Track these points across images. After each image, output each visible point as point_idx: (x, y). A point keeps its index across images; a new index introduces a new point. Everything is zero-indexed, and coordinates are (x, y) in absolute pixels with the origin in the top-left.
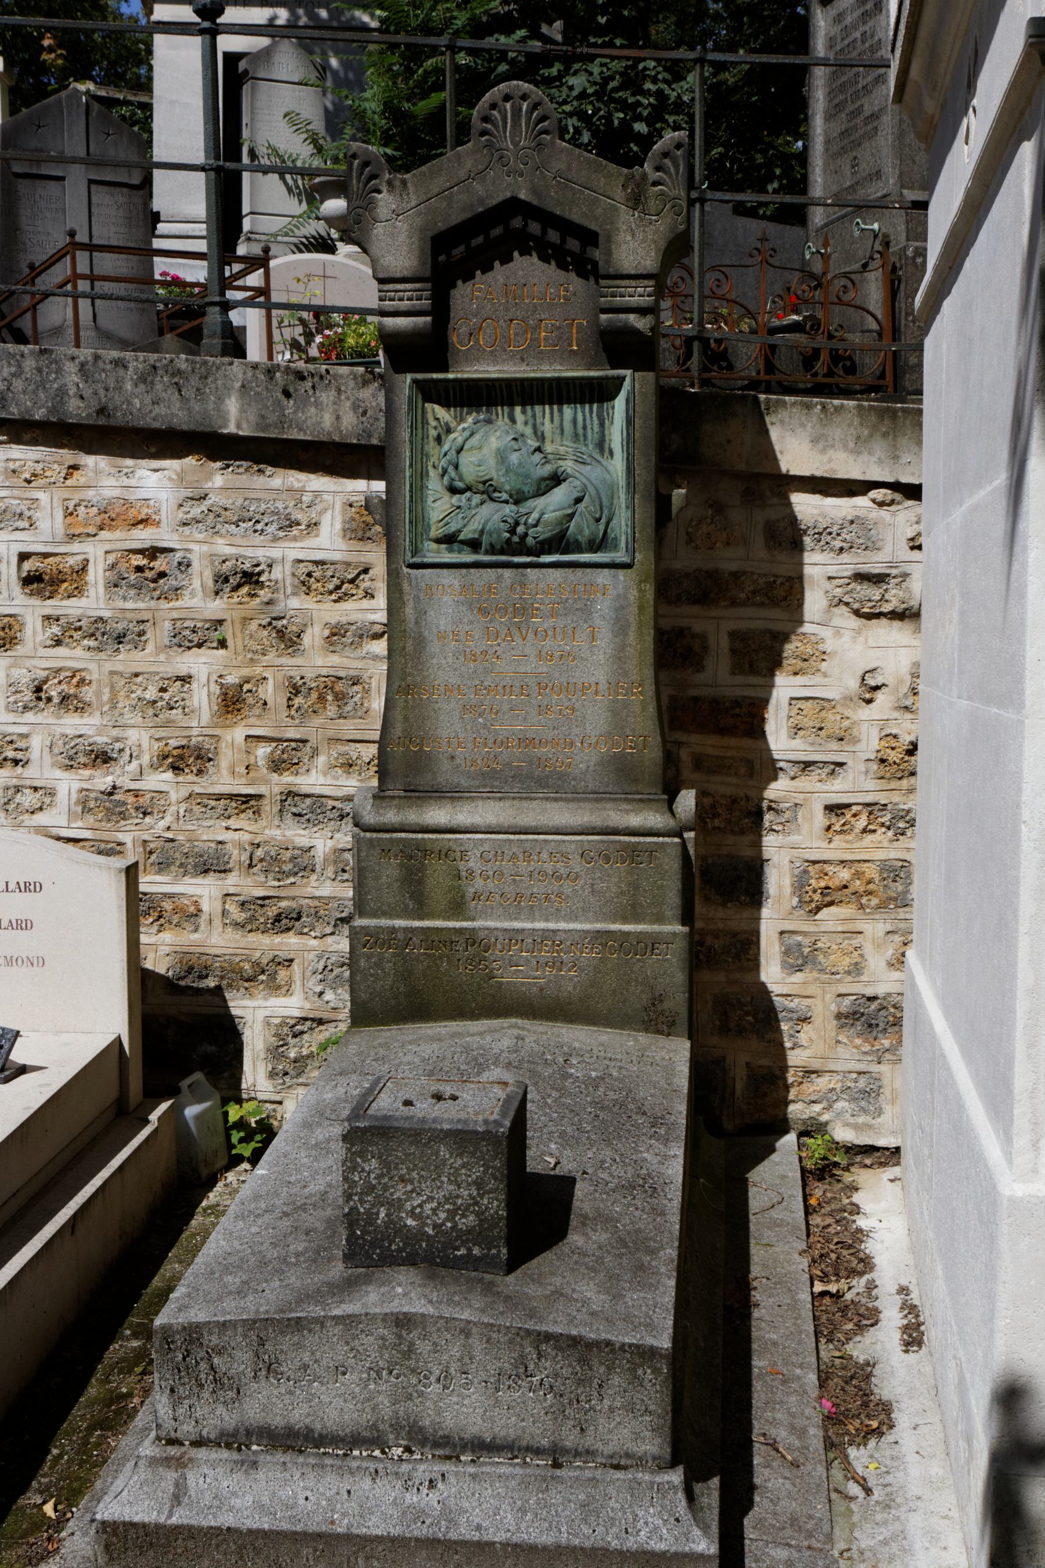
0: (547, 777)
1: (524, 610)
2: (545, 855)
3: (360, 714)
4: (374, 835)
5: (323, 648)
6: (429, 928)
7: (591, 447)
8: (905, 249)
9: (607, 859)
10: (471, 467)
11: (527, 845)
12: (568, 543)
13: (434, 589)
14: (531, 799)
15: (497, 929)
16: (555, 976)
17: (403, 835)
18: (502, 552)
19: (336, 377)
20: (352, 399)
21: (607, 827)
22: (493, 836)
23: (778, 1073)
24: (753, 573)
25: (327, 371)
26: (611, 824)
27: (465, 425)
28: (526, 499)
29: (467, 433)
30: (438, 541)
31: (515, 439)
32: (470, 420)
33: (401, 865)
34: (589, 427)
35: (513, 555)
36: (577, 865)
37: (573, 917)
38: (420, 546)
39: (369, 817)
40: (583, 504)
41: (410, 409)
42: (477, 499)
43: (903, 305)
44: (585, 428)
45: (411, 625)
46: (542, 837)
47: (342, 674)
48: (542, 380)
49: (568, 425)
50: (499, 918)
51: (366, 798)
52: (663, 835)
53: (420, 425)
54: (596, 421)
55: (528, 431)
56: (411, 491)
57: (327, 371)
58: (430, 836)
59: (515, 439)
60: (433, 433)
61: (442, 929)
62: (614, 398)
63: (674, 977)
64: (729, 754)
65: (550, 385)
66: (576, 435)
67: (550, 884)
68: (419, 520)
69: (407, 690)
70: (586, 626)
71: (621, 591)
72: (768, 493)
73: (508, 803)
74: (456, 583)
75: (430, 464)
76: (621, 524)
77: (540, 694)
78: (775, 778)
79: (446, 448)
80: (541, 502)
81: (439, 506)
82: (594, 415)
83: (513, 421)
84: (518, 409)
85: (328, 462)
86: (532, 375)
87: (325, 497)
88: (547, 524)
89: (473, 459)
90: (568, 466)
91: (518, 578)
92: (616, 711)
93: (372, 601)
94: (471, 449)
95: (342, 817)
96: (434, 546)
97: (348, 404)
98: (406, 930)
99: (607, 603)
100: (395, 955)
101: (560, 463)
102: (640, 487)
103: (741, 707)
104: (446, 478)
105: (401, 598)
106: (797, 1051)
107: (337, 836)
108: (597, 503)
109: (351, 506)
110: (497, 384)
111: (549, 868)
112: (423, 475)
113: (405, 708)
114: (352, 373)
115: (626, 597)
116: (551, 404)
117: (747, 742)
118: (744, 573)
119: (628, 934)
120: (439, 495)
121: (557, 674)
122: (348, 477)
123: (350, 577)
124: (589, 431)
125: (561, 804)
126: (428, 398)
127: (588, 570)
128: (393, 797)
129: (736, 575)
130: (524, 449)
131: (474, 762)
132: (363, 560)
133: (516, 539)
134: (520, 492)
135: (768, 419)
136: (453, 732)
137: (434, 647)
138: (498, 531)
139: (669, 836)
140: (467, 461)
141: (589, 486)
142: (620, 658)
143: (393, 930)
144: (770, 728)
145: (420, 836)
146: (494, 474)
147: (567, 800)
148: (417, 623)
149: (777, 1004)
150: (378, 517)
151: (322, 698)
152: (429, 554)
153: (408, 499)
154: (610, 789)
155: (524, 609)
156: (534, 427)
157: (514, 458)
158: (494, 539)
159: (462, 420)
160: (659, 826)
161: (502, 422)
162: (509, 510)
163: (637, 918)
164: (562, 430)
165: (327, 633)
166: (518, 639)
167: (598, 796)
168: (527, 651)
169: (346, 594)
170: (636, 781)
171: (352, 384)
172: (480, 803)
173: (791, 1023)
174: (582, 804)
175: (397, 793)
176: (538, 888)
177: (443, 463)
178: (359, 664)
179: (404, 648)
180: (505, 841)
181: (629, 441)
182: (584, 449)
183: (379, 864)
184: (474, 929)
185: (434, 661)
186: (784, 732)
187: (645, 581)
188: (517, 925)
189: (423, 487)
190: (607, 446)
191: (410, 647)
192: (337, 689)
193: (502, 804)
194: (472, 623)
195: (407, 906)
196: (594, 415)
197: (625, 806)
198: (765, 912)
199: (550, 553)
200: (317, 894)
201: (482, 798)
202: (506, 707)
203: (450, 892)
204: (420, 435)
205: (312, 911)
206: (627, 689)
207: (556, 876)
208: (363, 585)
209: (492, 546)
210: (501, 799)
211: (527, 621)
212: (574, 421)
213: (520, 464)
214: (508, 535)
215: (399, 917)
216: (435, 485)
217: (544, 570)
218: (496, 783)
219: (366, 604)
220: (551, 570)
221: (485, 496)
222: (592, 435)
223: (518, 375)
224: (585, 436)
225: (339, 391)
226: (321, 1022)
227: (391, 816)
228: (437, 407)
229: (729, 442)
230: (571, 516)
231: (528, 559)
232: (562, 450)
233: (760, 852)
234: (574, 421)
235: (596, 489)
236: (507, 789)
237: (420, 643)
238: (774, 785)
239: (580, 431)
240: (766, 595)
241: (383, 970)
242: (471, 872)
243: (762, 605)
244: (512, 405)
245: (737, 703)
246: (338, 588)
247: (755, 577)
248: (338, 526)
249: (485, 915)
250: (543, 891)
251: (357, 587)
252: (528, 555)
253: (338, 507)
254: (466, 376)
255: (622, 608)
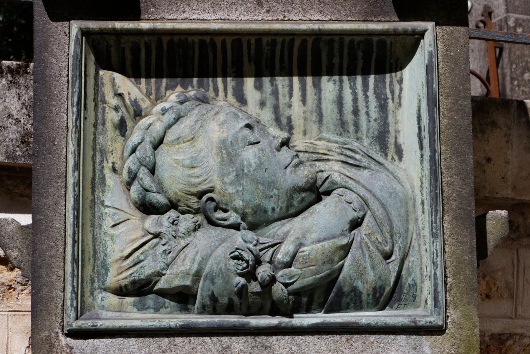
7: (366, 142)
8: (506, 19)
10: (176, 171)
12: (340, 293)
18: (230, 309)
24: (522, 336)
27: (167, 105)
28: (269, 222)
29: (169, 117)
30: (121, 292)
31: (249, 126)
34: (363, 111)
35: (247, 315)
38: (89, 300)
40: (364, 229)
42: (187, 222)
44: (356, 112)
48: (292, 34)
53: (91, 104)
54: (373, 102)
55: (266, 116)
56: (76, 208)
59: (249, 126)
60: (112, 117)
62: (402, 67)
65: (304, 43)
66: (343, 124)
68: (88, 255)
75: (108, 166)
79: (134, 138)
80: (295, 226)
81: (122, 235)
83: (242, 100)
84: (249, 82)
86: (277, 26)
88: (307, 262)
89: (180, 157)
90: (334, 170)
94: (177, 141)
96: (113, 299)
101: (320, 165)
104: (135, 187)
110: (218, 40)
112: (96, 183)
116: (302, 74)
118: (511, 336)
120: (122, 216)
124: (363, 117)
126: (104, 63)
127: (372, 338)
130: (264, 143)
133: (255, 287)
134: (259, 210)
138: (225, 274)
146: (217, 183)
152: (104, 314)
153: (70, 220)
156: (276, 109)
157: (250, 155)
158: (218, 287)
159: (159, 98)
162: (240, 239)
164: (320, 116)
177: (131, 163)
181: (432, 134)
182: (355, 145)
190: (391, 140)
199: (308, 310)
204: (91, 119)
209: (213, 298)
212: (340, 102)
213: (260, 164)
214: (242, 281)
216: (115, 198)
220: (310, 338)
221: (200, 218)
222: (368, 124)
223: (253, 26)
228: (118, 77)
229: (489, 160)
230: (346, 249)
232: (322, 146)
234: (340, 102)
235: (383, 205)
239: (349, 117)
244: (239, 74)
252: (273, 313)
254: (169, 26)
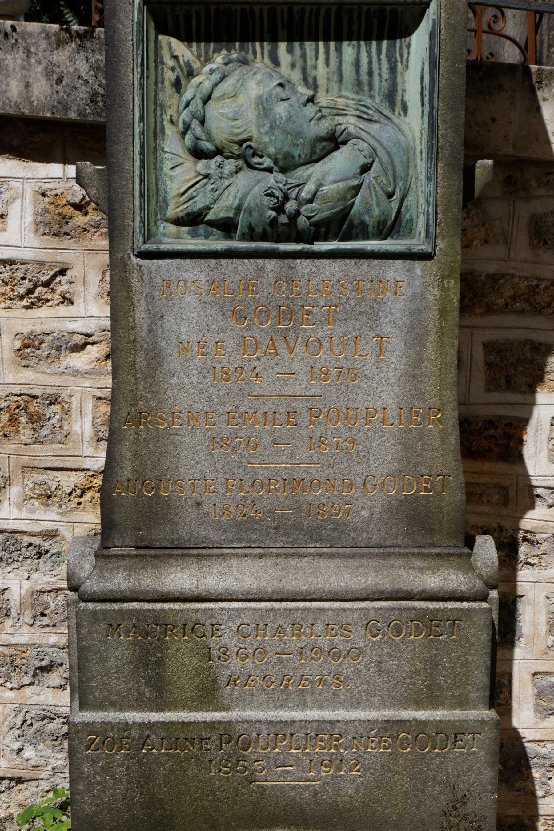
0: (319, 527)
1: (290, 314)
2: (319, 628)
3: (59, 438)
4: (99, 606)
5: (14, 362)
6: (172, 723)
7: (378, 99)
9: (398, 630)
10: (223, 120)
11: (297, 615)
12: (351, 225)
13: (173, 286)
14: (300, 556)
15: (259, 722)
16: (333, 777)
17: (136, 605)
18: (264, 237)
19: (24, 35)
20: (44, 63)
21: (398, 591)
22: (253, 605)
23: (527, 822)
24: (513, 276)
25: (13, 28)
26: (403, 587)
27: (214, 66)
28: (296, 166)
29: (216, 76)
30: (178, 222)
31: (281, 85)
32: (219, 59)
33: (134, 643)
35: (277, 242)
36: (359, 637)
37: (354, 702)
38: (154, 229)
39: (92, 585)
40: (372, 173)
41: (140, 40)
42: (230, 165)
43: (545, 38)
44: (370, 73)
45: (143, 334)
46: (315, 604)
47: (37, 392)
49: (348, 69)
50: (260, 707)
51: (83, 554)
52: (468, 600)
53: (152, 65)
54: (385, 65)
55: (296, 76)
56: (142, 153)
57: (13, 28)
58: (172, 606)
59: (281, 85)
60: (170, 76)
61: (189, 724)
63: (481, 773)
64: (482, 480)
66: (359, 83)
67: (325, 662)
68: (152, 194)
69: (139, 418)
70: (372, 334)
71: (418, 290)
72: (533, 183)
73: (269, 562)
74: (203, 278)
75: (167, 118)
76: (420, 201)
77: (311, 423)
78: (532, 507)
79: (188, 95)
80: (316, 170)
81: (179, 175)
82: (383, 57)
83: (276, 62)
84: (282, 46)
85: (15, 142)
87: (13, 183)
88: (325, 199)
90: (350, 123)
91: (284, 272)
92: (408, 446)
93: (71, 308)
94: (223, 97)
95: (40, 555)
97: (40, 69)
98: (142, 725)
99: (400, 305)
100: (127, 757)
101: (339, 119)
102: (446, 153)
103: (496, 428)
104: (188, 137)
105: (129, 297)
106: (548, 799)
107: (35, 576)
108: (390, 173)
109: (43, 195)
111: (324, 642)
112: (157, 133)
113: (136, 442)
114: (44, 30)
115: (423, 298)
116: (326, 39)
117: (501, 467)
118: (503, 275)
119: (425, 723)
120: (180, 161)
121: (334, 398)
122: (39, 161)
123: (44, 279)
124: (376, 78)
125: (338, 561)
127: (376, 262)
128: (122, 556)
129: (494, 278)
130: (293, 99)
131: (225, 510)
132: (59, 259)
133: (283, 219)
134: (288, 156)
135: (540, 94)
136: (198, 470)
137: (174, 362)
138: (260, 208)
139: (475, 600)
140: (216, 112)
141: (380, 150)
142: (414, 377)
143: (126, 726)
144: (528, 451)
145: (158, 606)
147: (346, 556)
148: (150, 330)
149: (528, 751)
150: (93, 192)
151: (13, 421)
152: (165, 240)
153: (137, 163)
154: (399, 542)
155: (291, 311)
156: (304, 70)
157: (281, 109)
159: (208, 60)
160: (464, 588)
161: (262, 63)
162: (274, 180)
163: (433, 702)
164: (341, 76)
165: (18, 344)
166: (282, 350)
167: (384, 551)
168: (295, 368)
169: (39, 299)
170: (431, 531)
171: (43, 44)
172: (234, 562)
173: (543, 770)
174: (364, 562)
175: (126, 551)
176: (312, 668)
177: (185, 115)
178: (57, 381)
179: (134, 364)
180: (269, 610)
181: (432, 92)
182: (369, 102)
183: (106, 642)
184: (230, 722)
185: (174, 380)
186: (544, 456)
187: (449, 277)
188: (285, 715)
189: (156, 149)
190: (399, 98)
191: (141, 361)
192: (32, 409)
193: (262, 562)
194: (223, 330)
195: (142, 694)
196: (383, 57)
197: (418, 563)
198: (518, 652)
199: (326, 239)
200: (13, 641)
201: (237, 555)
202: (267, 440)
203: (198, 675)
204: (152, 78)
205: (8, 660)
206: (422, 416)
207: (334, 653)
208: (60, 289)
209: (251, 228)
210: (261, 556)
211: (295, 327)
212: (357, 64)
213: (289, 117)
214: (273, 213)
215: (132, 708)
216: (172, 145)
217: (318, 262)
218: (254, 537)
219: (63, 310)
221: (241, 162)
222: (380, 84)
224: (370, 85)
225: (28, 53)
226: (19, 780)
227: (119, 581)
228: (174, 41)
229: (494, 120)
230: (357, 189)
231: (298, 247)
232: (341, 102)
233: (515, 587)
234: (357, 64)
235: (389, 154)
236: (268, 543)
237: (155, 357)
238: (530, 514)
239: (364, 77)
240: (527, 301)
241: (113, 776)
242: (225, 651)
243: (522, 312)
244: (274, 40)
245: (491, 423)
246: (30, 292)
247: (516, 280)
248: (29, 218)
249: (243, 702)
250: (317, 671)
251: (53, 291)
252: (298, 241)
253: (29, 195)
255: (419, 311)
